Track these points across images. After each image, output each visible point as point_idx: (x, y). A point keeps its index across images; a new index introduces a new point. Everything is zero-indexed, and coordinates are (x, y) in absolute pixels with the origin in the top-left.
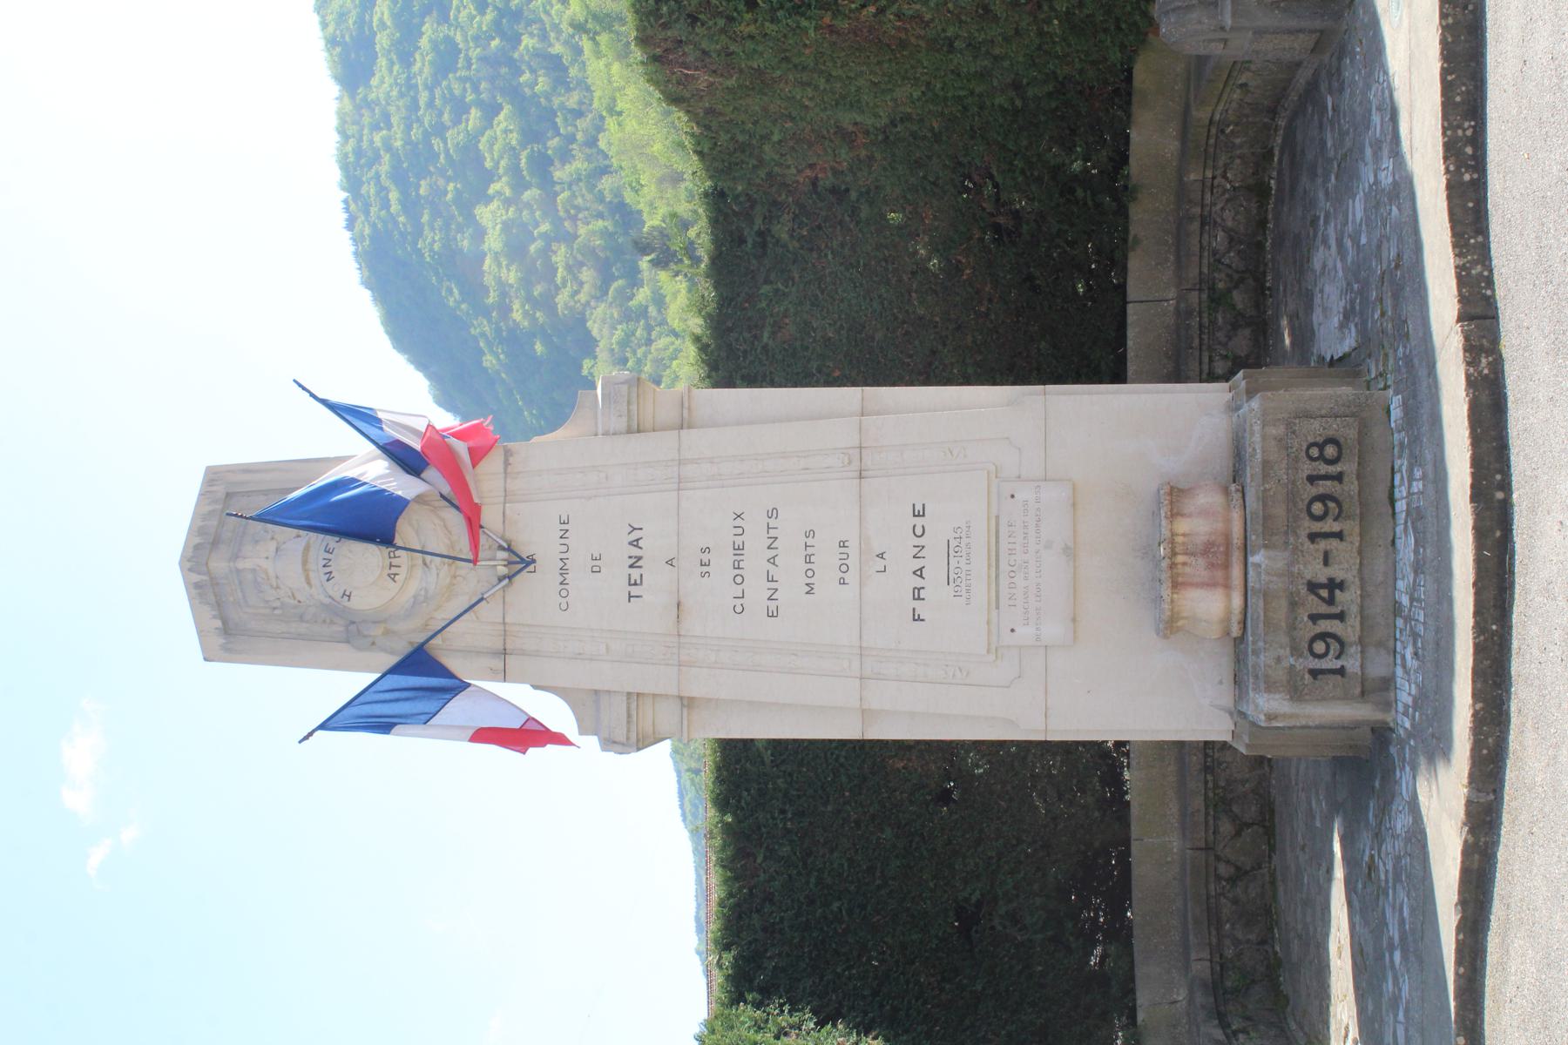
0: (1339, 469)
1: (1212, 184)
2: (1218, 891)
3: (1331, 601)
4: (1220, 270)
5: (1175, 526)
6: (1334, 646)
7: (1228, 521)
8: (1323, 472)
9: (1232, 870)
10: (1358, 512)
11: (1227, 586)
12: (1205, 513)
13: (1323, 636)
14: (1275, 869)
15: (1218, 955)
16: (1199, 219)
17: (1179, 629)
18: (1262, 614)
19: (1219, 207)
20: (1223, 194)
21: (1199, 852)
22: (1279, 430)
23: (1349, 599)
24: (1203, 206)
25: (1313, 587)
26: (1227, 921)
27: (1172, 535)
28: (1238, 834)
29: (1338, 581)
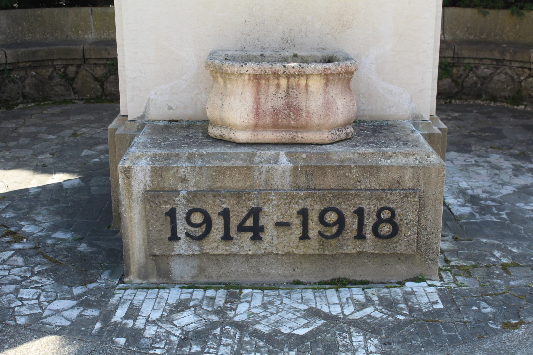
0: (368, 236)
1: (525, 68)
2: (57, 67)
3: (241, 228)
4: (465, 70)
5: (315, 77)
6: (199, 231)
7: (319, 128)
8: (366, 221)
9: (72, 75)
10: (327, 253)
11: (256, 127)
12: (328, 106)
13: (208, 221)
14: (74, 103)
15: (11, 68)
16: (501, 58)
17: (215, 78)
18: (229, 164)
19: (509, 71)
20: (517, 75)
21: (82, 54)
22: (408, 182)
23: (244, 245)
24: (510, 61)
25: (255, 213)
26: (37, 73)
27: (307, 75)
28: (96, 79)
29: (261, 235)
